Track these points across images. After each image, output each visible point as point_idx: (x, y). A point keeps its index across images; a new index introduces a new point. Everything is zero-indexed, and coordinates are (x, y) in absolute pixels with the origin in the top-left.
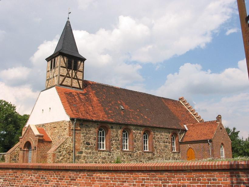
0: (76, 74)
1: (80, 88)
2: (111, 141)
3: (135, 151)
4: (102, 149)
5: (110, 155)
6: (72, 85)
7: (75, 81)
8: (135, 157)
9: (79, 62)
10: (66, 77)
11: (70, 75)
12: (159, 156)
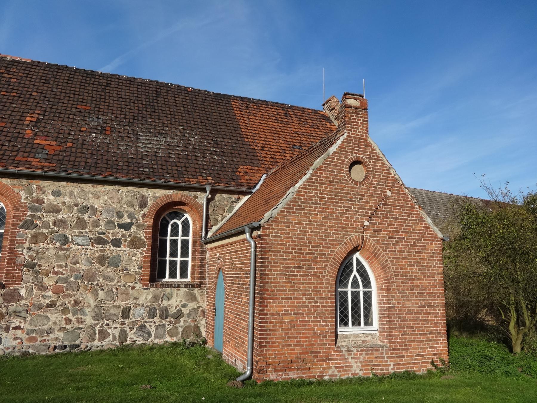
12: (52, 305)
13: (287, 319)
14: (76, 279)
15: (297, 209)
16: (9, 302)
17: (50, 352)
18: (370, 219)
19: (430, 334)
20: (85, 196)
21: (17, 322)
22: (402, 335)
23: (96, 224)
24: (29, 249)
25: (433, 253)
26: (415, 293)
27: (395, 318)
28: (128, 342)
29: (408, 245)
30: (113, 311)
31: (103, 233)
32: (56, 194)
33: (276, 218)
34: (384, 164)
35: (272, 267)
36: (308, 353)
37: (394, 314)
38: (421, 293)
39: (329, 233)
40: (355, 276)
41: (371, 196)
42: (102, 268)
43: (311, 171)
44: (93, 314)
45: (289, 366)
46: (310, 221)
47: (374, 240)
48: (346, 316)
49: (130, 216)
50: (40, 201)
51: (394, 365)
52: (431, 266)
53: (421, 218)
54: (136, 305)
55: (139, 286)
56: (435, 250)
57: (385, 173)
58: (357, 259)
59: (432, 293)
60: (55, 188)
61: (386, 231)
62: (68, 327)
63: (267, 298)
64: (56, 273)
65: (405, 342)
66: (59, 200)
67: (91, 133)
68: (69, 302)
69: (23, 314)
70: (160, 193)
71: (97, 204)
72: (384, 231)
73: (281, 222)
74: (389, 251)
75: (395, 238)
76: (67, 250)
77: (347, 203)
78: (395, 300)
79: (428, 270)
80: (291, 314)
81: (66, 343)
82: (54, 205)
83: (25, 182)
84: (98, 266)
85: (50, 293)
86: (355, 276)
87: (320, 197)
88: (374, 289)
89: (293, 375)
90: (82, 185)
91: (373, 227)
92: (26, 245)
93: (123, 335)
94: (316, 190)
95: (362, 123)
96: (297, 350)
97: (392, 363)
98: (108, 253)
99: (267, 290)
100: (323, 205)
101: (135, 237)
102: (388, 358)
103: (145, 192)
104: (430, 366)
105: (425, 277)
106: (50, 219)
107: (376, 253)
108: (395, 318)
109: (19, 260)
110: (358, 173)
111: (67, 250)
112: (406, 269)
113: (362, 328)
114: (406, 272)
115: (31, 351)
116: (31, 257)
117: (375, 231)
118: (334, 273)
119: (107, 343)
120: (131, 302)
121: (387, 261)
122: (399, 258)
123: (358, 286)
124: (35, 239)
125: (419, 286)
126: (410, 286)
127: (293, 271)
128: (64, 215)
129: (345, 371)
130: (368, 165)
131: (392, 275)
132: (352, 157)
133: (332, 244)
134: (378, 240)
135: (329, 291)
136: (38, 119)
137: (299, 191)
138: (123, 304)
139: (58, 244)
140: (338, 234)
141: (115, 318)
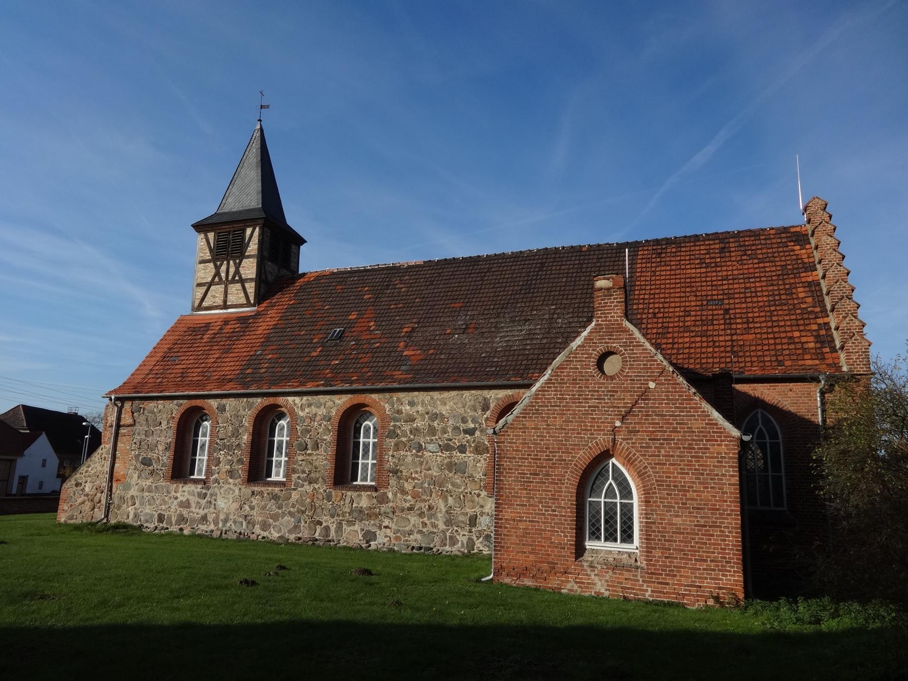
0: (238, 267)
1: (248, 304)
2: (215, 451)
3: (297, 484)
4: (359, 482)
5: (206, 494)
6: (225, 301)
7: (235, 288)
8: (293, 506)
9: (249, 231)
10: (210, 284)
11: (223, 275)
12: (411, 509)
13: (522, 526)
14: (429, 485)
15: (533, 414)
16: (381, 504)
17: (409, 551)
18: (622, 420)
19: (711, 561)
20: (434, 403)
21: (386, 522)
22: (667, 557)
23: (444, 431)
24: (393, 456)
25: (722, 457)
26: (689, 508)
27: (657, 536)
28: (475, 551)
29: (680, 448)
30: (461, 518)
31: (451, 440)
32: (412, 404)
33: (512, 424)
34: (646, 349)
35: (507, 473)
36: (544, 562)
37: (654, 532)
38: (698, 509)
39: (571, 437)
40: (611, 484)
41: (626, 390)
42: (451, 475)
43: (550, 372)
44: (444, 520)
45: (524, 572)
46: (548, 425)
47: (628, 443)
48: (599, 530)
49: (474, 421)
50: (399, 412)
51: (652, 591)
52: (717, 475)
53: (704, 412)
54: (482, 514)
55: (484, 493)
56: (725, 453)
57: (647, 361)
58: (613, 464)
59: (718, 509)
60: (410, 399)
61: (645, 431)
62: (425, 530)
63: (502, 504)
64: (413, 479)
65: (670, 567)
66: (414, 409)
67: (454, 334)
68: (424, 506)
69: (391, 515)
70: (502, 394)
71: (444, 410)
72: (642, 432)
73: (516, 428)
74: (650, 456)
75: (659, 440)
76: (421, 457)
77: (592, 402)
78: (657, 514)
79: (711, 479)
80: (526, 521)
81: (423, 545)
82: (410, 415)
83: (387, 395)
84: (447, 472)
85: (409, 497)
86: (611, 484)
87: (560, 399)
88: (636, 501)
89: (528, 582)
90: (431, 393)
91: (627, 428)
92: (391, 453)
93: (471, 544)
94: (555, 391)
95: (615, 306)
96: (532, 557)
97: (649, 589)
98: (455, 460)
99: (502, 496)
100: (564, 406)
101: (479, 442)
102: (643, 581)
103: (487, 394)
104: (711, 602)
105: (707, 488)
106: (407, 428)
107: (631, 458)
108: (657, 536)
109: (387, 466)
110: (612, 365)
111: (421, 457)
112: (674, 477)
113: (618, 546)
114: (675, 482)
115: (396, 549)
116: (394, 463)
117: (630, 432)
118: (575, 481)
119: (455, 549)
120: (478, 510)
121: (646, 467)
122: (665, 464)
123: (615, 497)
124: (397, 447)
125: (696, 500)
126: (682, 499)
127: (529, 478)
128: (419, 423)
129: (588, 588)
130: (624, 354)
131: (653, 484)
132: (601, 348)
133: (573, 449)
134: (633, 443)
135: (569, 500)
136: (413, 328)
137: (536, 395)
138: (470, 512)
139: (414, 451)
140: (581, 438)
141: (463, 525)
